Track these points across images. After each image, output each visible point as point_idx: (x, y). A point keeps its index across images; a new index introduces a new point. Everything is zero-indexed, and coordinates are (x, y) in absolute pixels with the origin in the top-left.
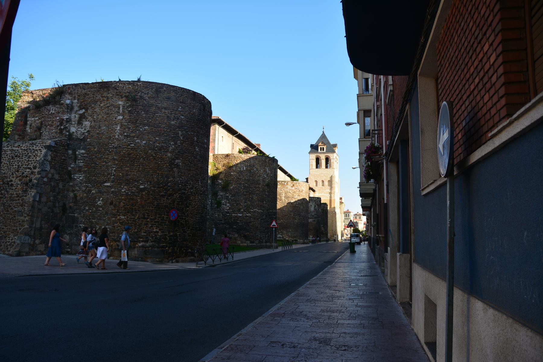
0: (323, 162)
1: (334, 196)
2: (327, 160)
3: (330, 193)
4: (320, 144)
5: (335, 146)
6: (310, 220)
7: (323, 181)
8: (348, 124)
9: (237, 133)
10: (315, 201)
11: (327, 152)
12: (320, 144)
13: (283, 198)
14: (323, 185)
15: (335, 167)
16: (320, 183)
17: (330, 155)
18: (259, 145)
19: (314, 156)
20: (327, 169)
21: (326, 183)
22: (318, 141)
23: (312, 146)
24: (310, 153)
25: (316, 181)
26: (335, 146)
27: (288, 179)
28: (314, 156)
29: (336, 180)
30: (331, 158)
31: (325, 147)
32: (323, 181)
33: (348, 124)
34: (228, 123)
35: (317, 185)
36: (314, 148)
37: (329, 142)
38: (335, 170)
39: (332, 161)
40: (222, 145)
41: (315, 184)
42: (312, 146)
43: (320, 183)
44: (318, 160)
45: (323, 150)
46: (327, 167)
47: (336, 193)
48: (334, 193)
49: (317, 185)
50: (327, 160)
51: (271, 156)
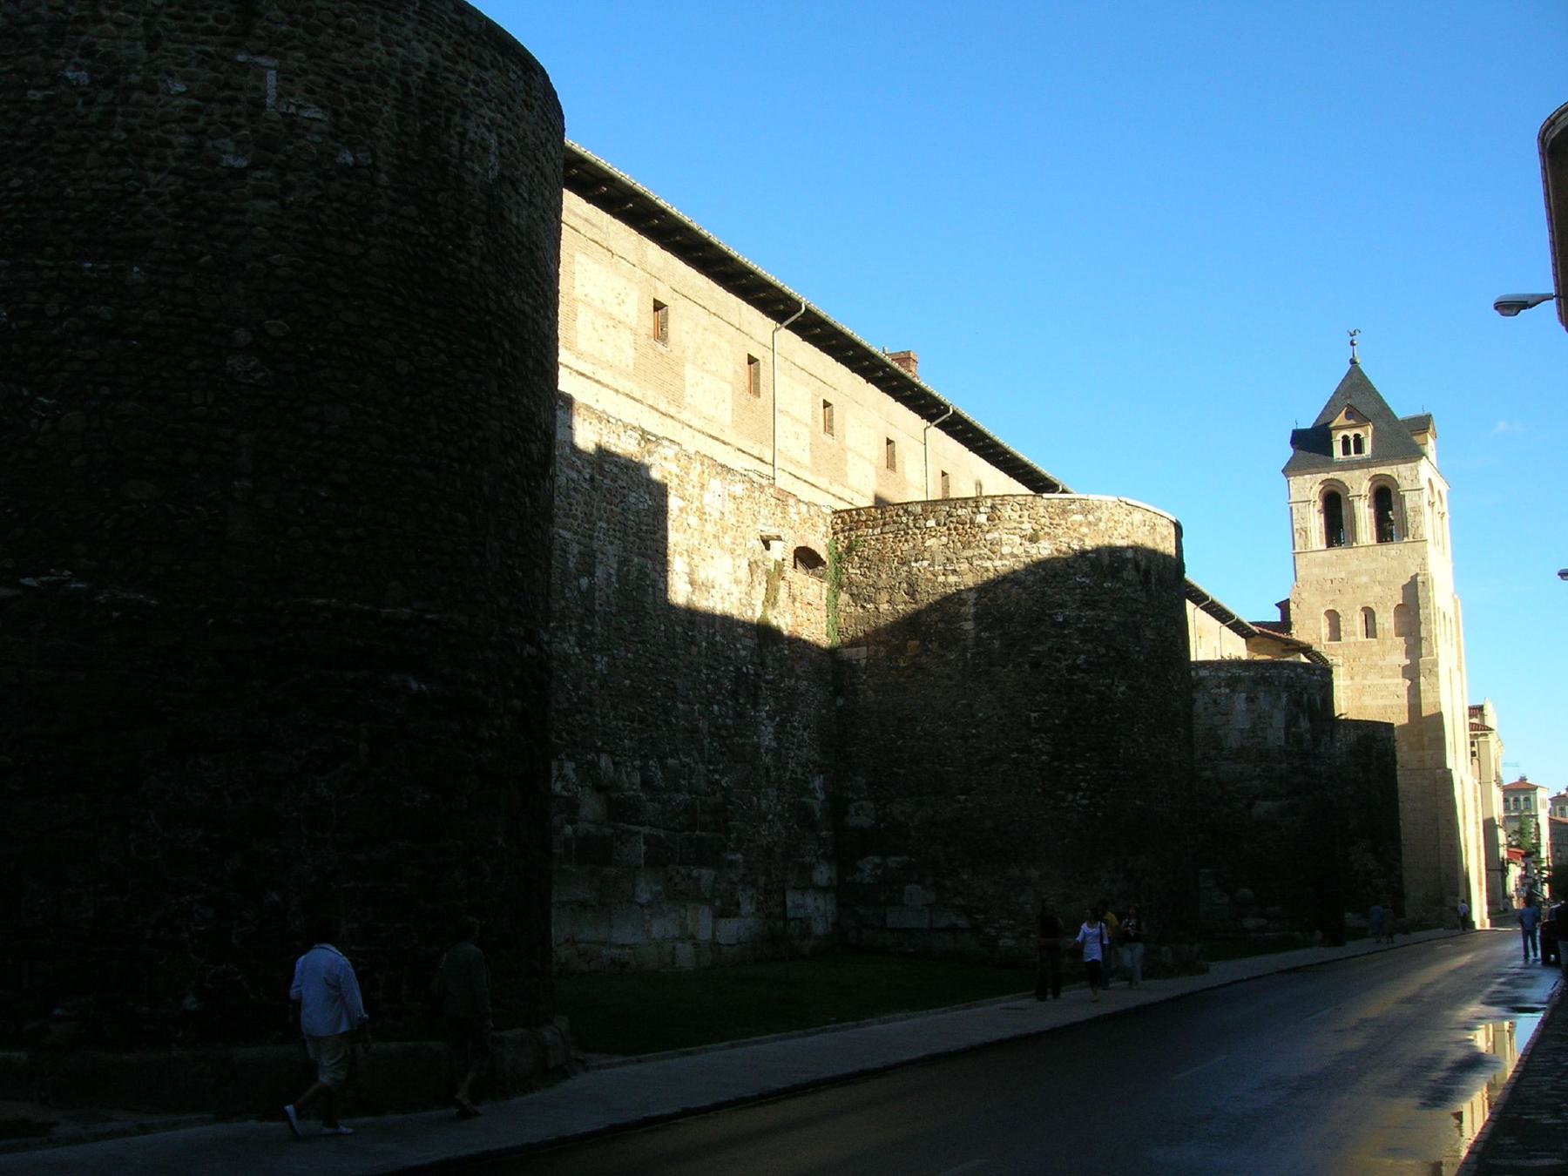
0: (1364, 515)
1: (1435, 688)
2: (1384, 497)
3: (1412, 673)
4: (1340, 420)
5: (1422, 424)
6: (1262, 807)
7: (1369, 614)
8: (1510, 307)
9: (1207, 598)
10: (1289, 686)
11: (1379, 458)
12: (1340, 420)
13: (969, 626)
14: (1370, 631)
15: (1427, 532)
16: (1354, 624)
17: (1399, 472)
18: (905, 359)
19: (1310, 486)
20: (1384, 548)
21: (1386, 620)
22: (1330, 409)
23: (1301, 440)
24: (1291, 469)
25: (1333, 616)
26: (1422, 424)
27: (998, 482)
28: (1310, 486)
29: (1442, 598)
30: (1404, 485)
31: (1367, 434)
32: (1369, 614)
33: (1510, 307)
34: (814, 307)
35: (1335, 634)
36: (1311, 444)
37: (1385, 412)
38: (1430, 547)
39: (1408, 504)
40: (1209, 642)
41: (1325, 630)
42: (1301, 440)
43: (1354, 624)
44: (1334, 506)
45: (1359, 449)
46: (1385, 533)
47: (1443, 669)
48: (1433, 671)
49: (1335, 634)
50: (1384, 497)
51: (1449, 766)
